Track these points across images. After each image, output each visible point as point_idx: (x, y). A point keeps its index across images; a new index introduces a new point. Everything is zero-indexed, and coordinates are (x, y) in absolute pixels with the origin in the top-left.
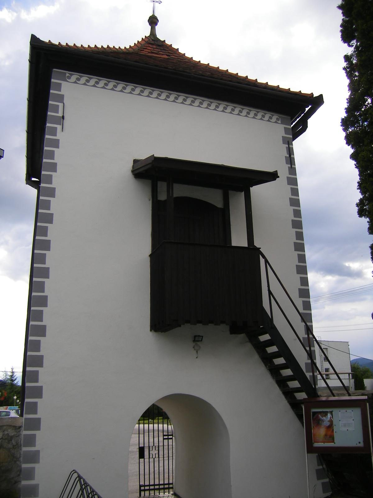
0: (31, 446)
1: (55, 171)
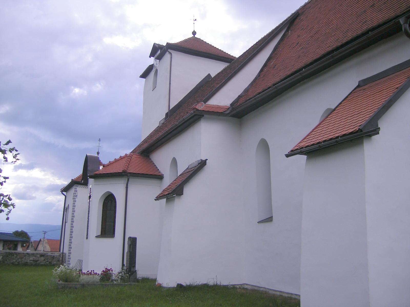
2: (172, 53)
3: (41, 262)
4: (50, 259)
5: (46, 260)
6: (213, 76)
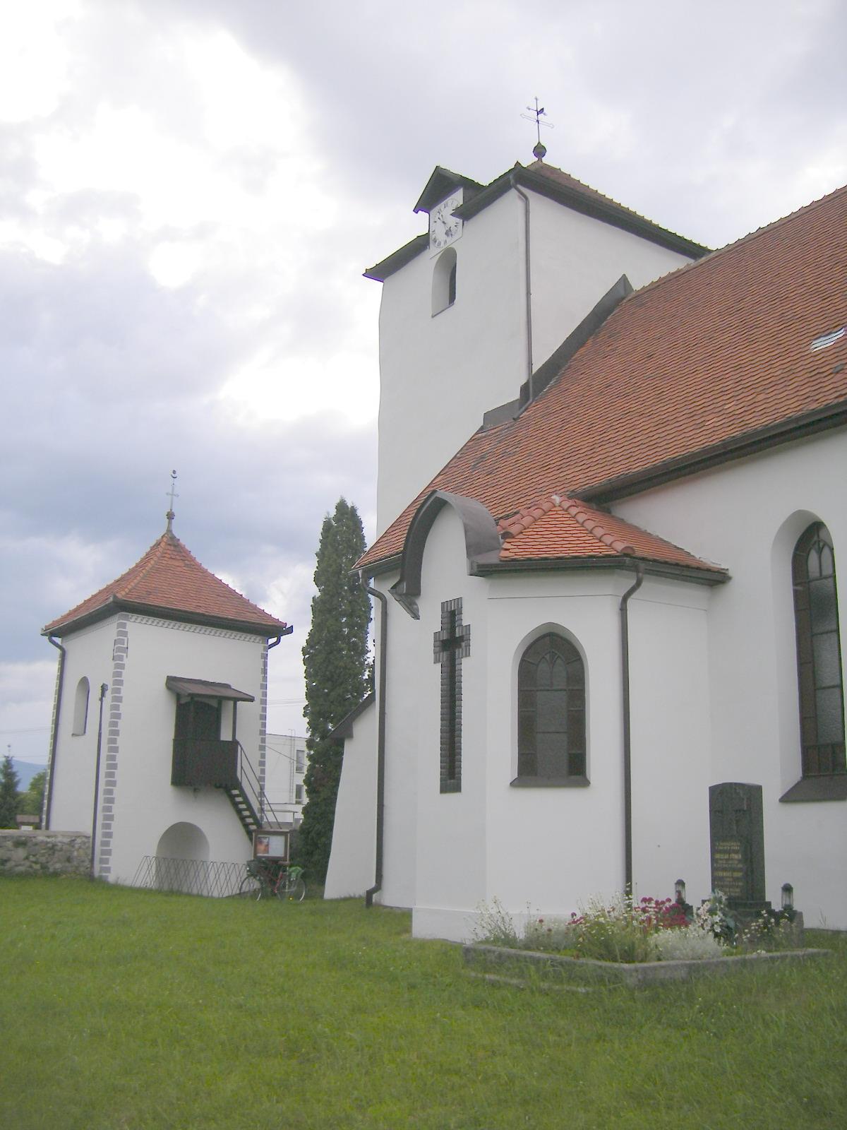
0: (106, 832)
1: (113, 820)
2: (529, 198)
3: (16, 866)
4: (43, 855)
5: (32, 858)
6: (637, 284)
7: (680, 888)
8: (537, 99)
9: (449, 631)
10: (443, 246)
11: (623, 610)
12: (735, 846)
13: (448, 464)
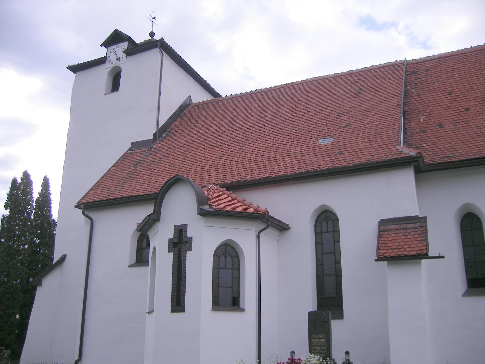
7: (292, 354)
8: (153, 12)
9: (178, 239)
10: (114, 65)
11: (258, 237)
12: (322, 336)
13: (117, 162)
